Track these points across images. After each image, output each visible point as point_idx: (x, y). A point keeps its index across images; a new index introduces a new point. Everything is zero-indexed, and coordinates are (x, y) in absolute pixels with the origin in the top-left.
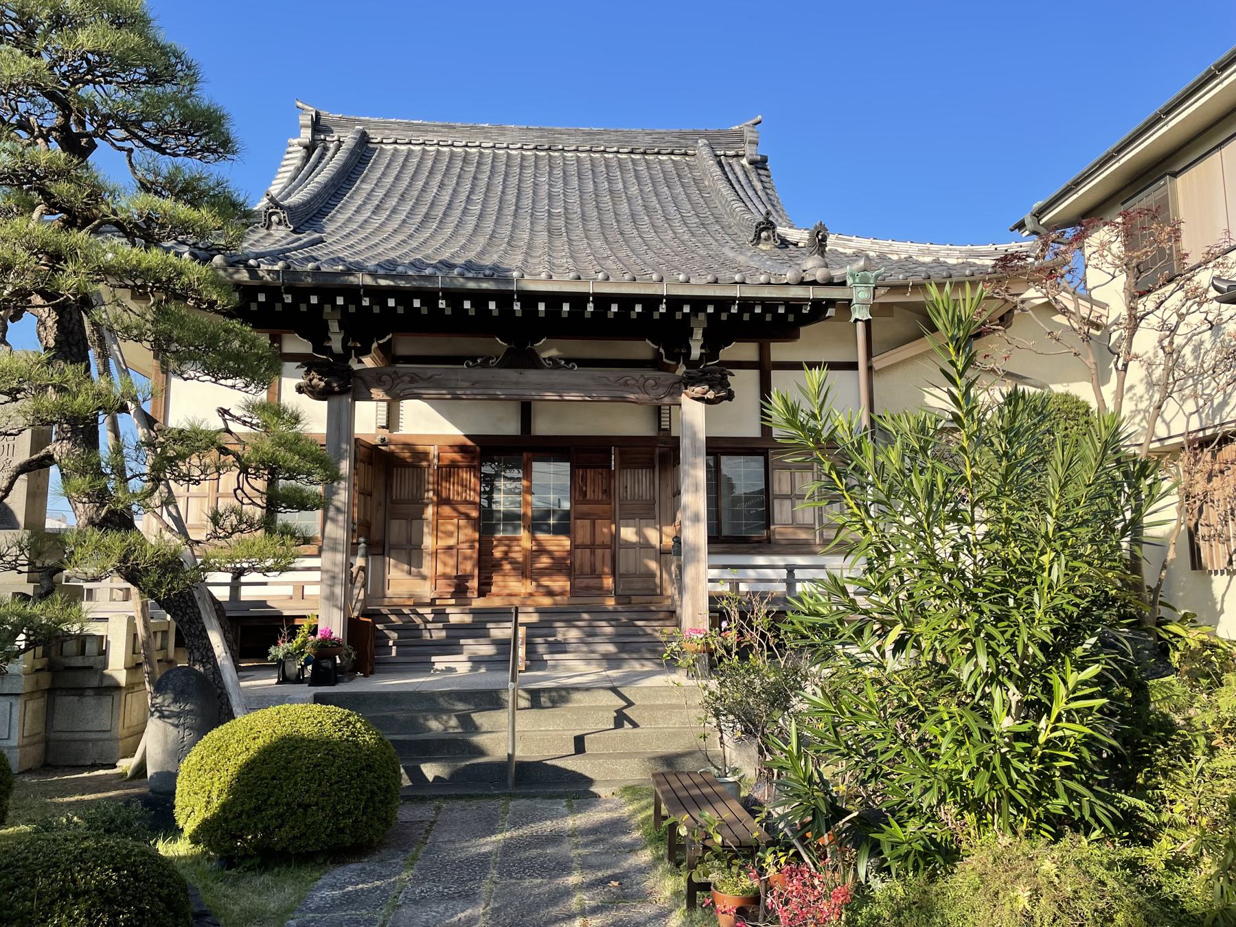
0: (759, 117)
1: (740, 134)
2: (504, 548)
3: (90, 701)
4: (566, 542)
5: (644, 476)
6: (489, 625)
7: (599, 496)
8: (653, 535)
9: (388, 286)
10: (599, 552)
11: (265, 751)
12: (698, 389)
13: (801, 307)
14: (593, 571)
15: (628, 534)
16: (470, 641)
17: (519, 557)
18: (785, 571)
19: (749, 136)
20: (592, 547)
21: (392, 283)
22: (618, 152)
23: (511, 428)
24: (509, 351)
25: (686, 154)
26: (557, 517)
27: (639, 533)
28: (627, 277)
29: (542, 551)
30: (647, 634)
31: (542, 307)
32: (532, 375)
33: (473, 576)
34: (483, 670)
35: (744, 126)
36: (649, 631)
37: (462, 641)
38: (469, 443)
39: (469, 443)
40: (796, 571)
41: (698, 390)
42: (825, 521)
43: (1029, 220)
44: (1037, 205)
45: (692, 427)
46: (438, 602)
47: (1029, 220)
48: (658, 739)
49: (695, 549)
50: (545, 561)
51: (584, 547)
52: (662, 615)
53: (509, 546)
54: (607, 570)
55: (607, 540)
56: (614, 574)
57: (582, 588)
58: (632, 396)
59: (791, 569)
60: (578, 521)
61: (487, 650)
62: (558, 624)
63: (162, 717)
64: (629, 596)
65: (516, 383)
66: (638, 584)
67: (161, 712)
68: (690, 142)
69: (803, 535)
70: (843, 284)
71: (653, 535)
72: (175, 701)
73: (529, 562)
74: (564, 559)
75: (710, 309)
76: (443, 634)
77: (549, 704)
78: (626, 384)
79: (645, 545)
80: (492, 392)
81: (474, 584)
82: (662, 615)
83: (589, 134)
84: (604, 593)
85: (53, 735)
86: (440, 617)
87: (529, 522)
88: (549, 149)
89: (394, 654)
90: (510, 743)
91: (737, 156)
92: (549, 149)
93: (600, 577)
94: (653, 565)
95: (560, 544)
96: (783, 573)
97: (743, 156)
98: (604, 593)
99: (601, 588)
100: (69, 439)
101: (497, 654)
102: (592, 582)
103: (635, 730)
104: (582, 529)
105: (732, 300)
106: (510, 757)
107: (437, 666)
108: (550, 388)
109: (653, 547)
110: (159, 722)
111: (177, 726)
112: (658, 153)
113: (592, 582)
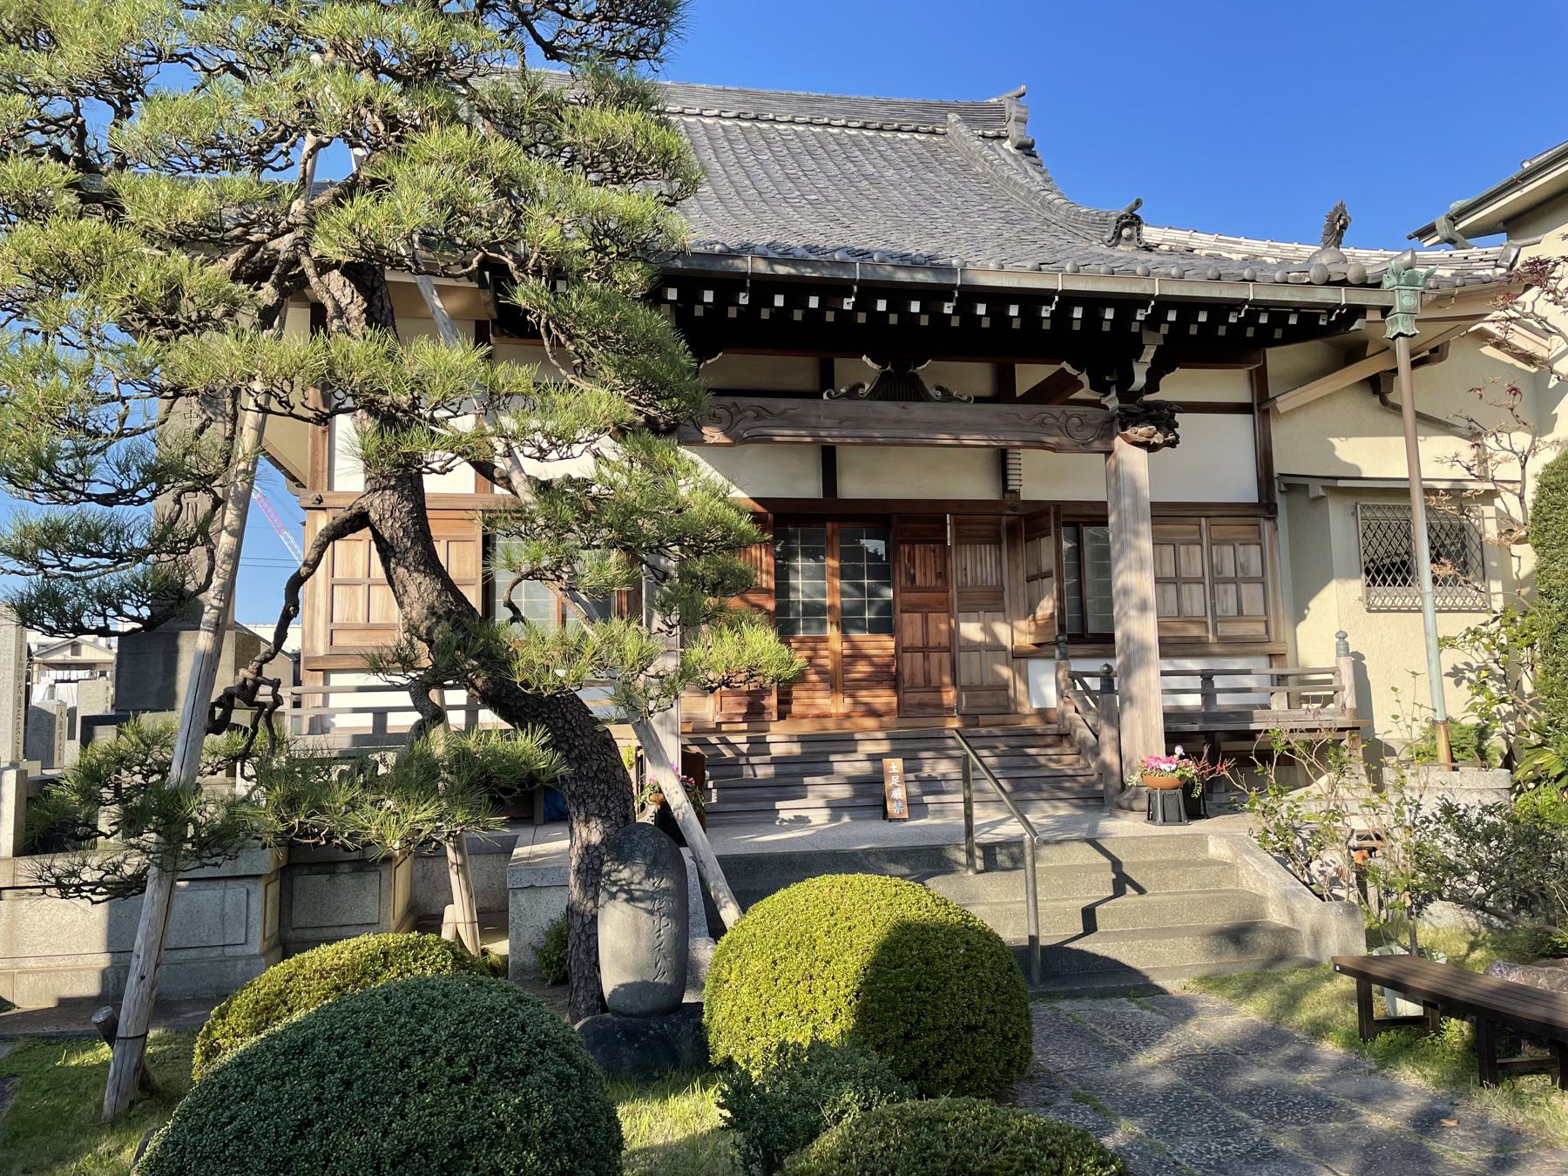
0: (1023, 88)
1: (1000, 109)
2: (808, 653)
3: (346, 881)
4: (888, 643)
5: (987, 553)
6: (832, 758)
7: (932, 580)
8: (1002, 631)
9: (789, 276)
10: (934, 656)
11: (884, 948)
12: (1143, 430)
13: (1287, 315)
14: (928, 681)
15: (971, 630)
16: (819, 780)
17: (827, 663)
18: (1199, 679)
19: (1013, 110)
20: (925, 650)
21: (793, 271)
22: (845, 126)
23: (809, 487)
24: (884, 377)
25: (933, 133)
26: (875, 608)
27: (987, 630)
28: (1103, 269)
29: (857, 655)
30: (1040, 766)
31: (1014, 311)
32: (918, 410)
33: (770, 692)
34: (846, 819)
35: (1005, 99)
36: (1042, 760)
37: (807, 780)
38: (759, 509)
39: (759, 509)
40: (1215, 678)
41: (1141, 431)
42: (1219, 612)
43: (1441, 223)
44: (1456, 205)
45: (1133, 481)
46: (724, 727)
47: (1441, 223)
48: (1190, 909)
49: (1143, 648)
50: (862, 668)
51: (912, 649)
52: (1049, 740)
53: (814, 650)
54: (947, 679)
55: (945, 641)
56: (954, 684)
57: (911, 705)
58: (1051, 440)
59: (1207, 677)
60: (906, 616)
61: (842, 792)
62: (924, 754)
63: (631, 899)
64: (976, 716)
65: (897, 422)
66: (986, 700)
67: (629, 892)
68: (937, 117)
69: (1195, 631)
70: (1378, 285)
71: (1002, 631)
72: (649, 875)
73: (839, 671)
74: (888, 666)
75: (1203, 317)
76: (771, 770)
77: (1009, 864)
78: (1042, 424)
79: (995, 647)
80: (867, 433)
81: (772, 701)
82: (1049, 740)
83: (807, 100)
84: (945, 711)
85: (291, 935)
86: (760, 748)
87: (838, 617)
88: (756, 118)
89: (714, 800)
90: (1032, 922)
91: (998, 137)
92: (756, 118)
93: (938, 690)
94: (1006, 672)
95: (881, 646)
96: (1196, 683)
97: (1006, 138)
98: (945, 711)
99: (940, 705)
100: (393, 488)
101: (855, 797)
102: (928, 697)
103: (1144, 898)
104: (912, 626)
105: (1235, 305)
106: (1033, 940)
107: (782, 815)
108: (944, 427)
109: (1004, 649)
110: (626, 908)
111: (651, 912)
112: (898, 130)
113: (928, 697)
